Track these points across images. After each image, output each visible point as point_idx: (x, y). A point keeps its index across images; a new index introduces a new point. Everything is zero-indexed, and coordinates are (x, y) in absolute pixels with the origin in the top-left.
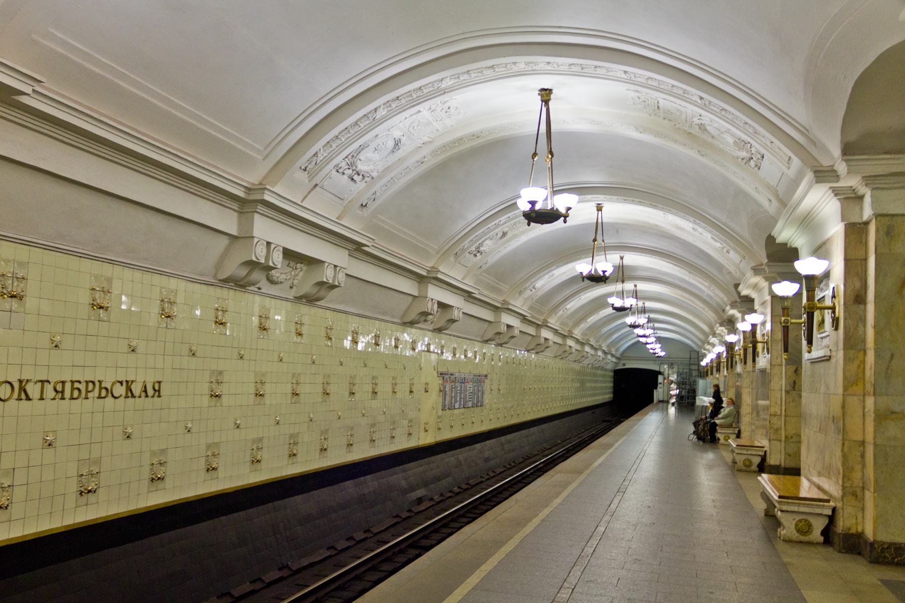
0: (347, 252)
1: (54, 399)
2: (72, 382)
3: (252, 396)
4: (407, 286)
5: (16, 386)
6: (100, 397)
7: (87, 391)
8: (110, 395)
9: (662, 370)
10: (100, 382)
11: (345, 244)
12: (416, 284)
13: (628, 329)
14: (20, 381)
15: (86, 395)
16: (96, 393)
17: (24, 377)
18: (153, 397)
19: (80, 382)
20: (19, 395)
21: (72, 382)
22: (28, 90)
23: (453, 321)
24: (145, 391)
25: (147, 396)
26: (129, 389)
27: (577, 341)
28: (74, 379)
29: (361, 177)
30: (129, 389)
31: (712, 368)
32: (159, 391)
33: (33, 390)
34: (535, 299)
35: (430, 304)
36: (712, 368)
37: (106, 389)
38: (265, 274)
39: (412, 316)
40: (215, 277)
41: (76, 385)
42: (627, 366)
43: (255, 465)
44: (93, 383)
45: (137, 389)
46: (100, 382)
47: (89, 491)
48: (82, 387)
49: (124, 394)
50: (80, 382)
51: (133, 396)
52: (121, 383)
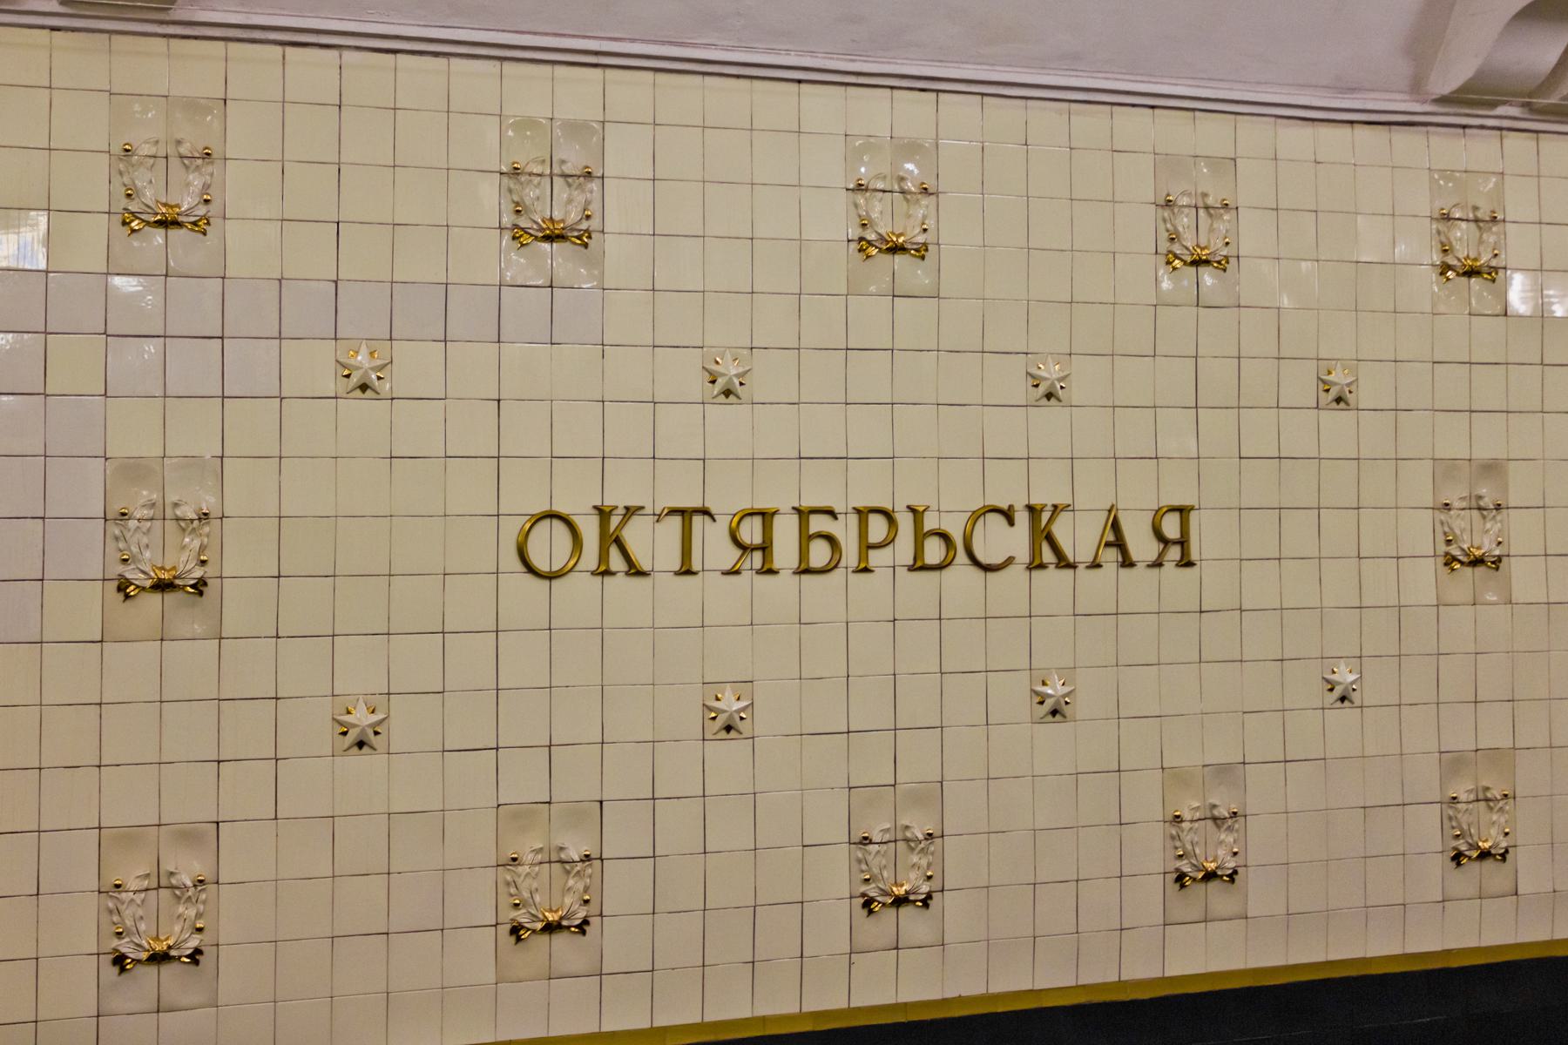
2: (803, 514)
6: (918, 566)
7: (866, 547)
8: (961, 557)
16: (904, 549)
17: (617, 498)
18: (1157, 564)
21: (803, 514)
24: (1119, 544)
26: (1043, 536)
33: (653, 542)
40: (1416, 87)
41: (818, 524)
44: (887, 515)
49: (1023, 555)
52: (1008, 515)
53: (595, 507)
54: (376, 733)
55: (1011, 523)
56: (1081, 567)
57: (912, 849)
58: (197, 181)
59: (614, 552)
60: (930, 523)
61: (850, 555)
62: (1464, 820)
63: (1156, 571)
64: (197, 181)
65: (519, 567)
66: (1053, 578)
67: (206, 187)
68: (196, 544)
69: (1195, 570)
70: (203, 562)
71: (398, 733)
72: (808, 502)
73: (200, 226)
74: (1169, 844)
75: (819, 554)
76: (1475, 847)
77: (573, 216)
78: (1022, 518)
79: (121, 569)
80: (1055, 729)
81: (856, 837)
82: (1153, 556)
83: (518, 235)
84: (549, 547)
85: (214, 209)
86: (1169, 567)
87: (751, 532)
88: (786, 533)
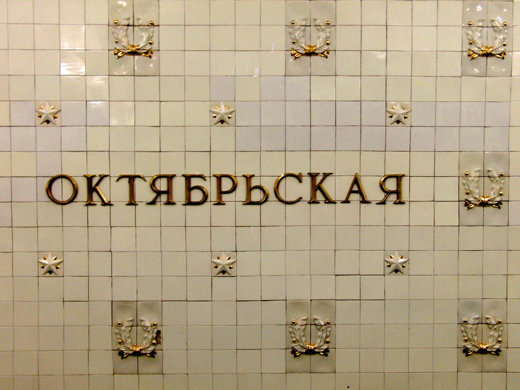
2: (188, 178)
6: (249, 202)
7: (221, 193)
10: (248, 178)
15: (220, 198)
16: (241, 193)
17: (96, 171)
20: (90, 197)
21: (188, 178)
26: (316, 188)
33: (114, 191)
38: (97, 188)
41: (195, 182)
46: (248, 178)
48: (210, 187)
49: (307, 197)
52: (299, 178)
53: (308, 174)
54: (403, 267)
55: (300, 181)
56: (338, 203)
57: (491, 329)
58: (323, 35)
59: (318, 193)
60: (255, 182)
61: (213, 196)
63: (383, 206)
64: (323, 35)
66: (322, 207)
67: (327, 38)
68: (498, 187)
69: (405, 207)
70: (501, 195)
71: (413, 268)
72: (189, 173)
73: (325, 54)
74: (289, 335)
75: (196, 196)
77: (497, 44)
78: (307, 181)
79: (466, 197)
81: (115, 323)
85: (331, 47)
86: (390, 204)
87: (162, 185)
88: (179, 185)
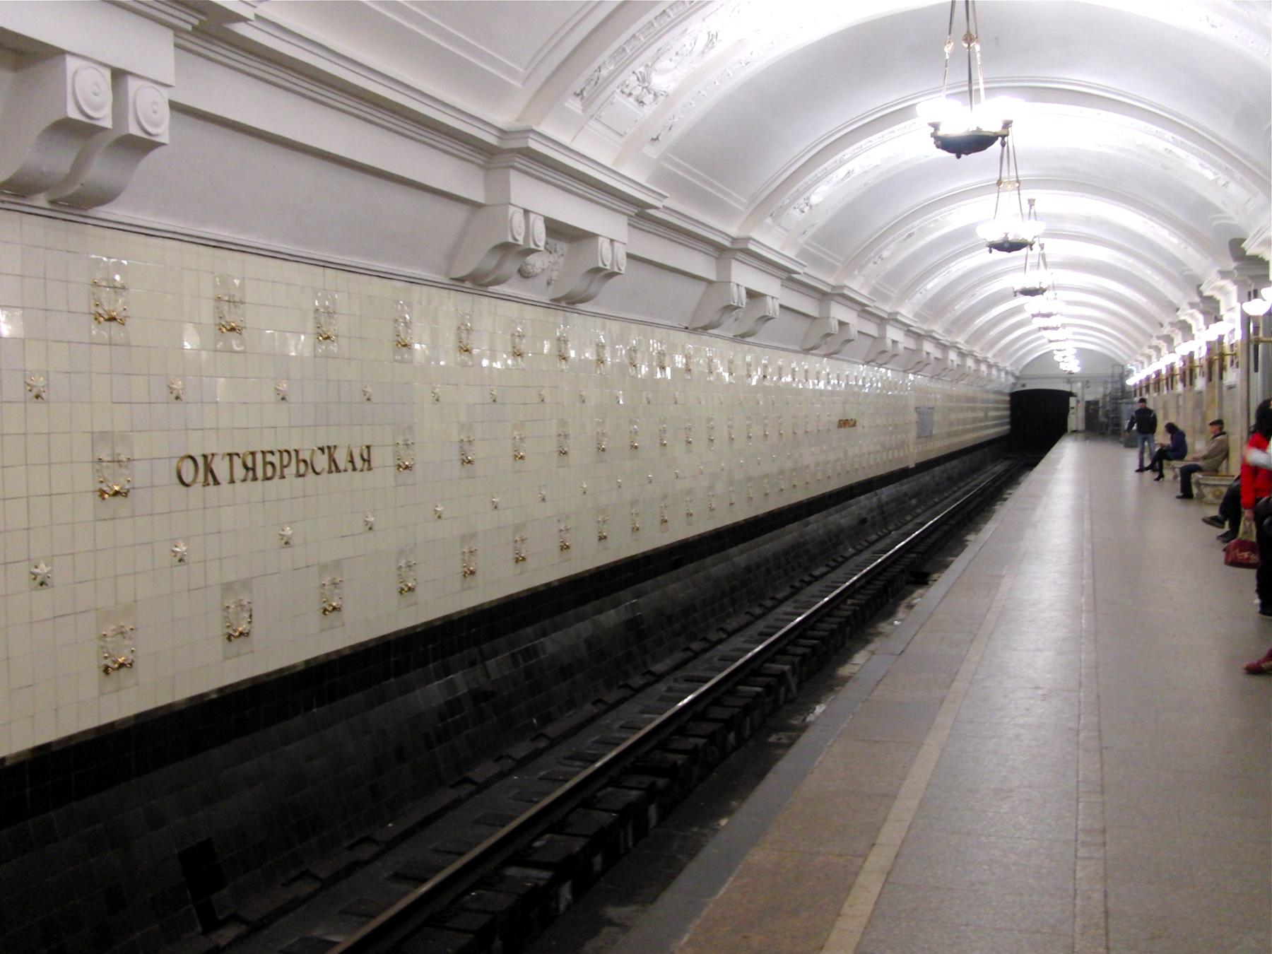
0: (168, 37)
1: (244, 480)
3: (392, 470)
4: (700, 264)
5: (200, 461)
6: (299, 475)
7: (283, 467)
8: (310, 470)
9: (1074, 391)
11: (779, 273)
12: (713, 262)
13: (985, 257)
14: (205, 457)
15: (282, 472)
17: (208, 452)
18: (244, 480)
19: (272, 453)
22: (659, 204)
23: (766, 319)
24: (352, 461)
25: (354, 469)
26: (332, 460)
27: (909, 331)
28: (265, 449)
29: (651, 96)
30: (332, 460)
31: (1141, 389)
32: (369, 461)
33: (220, 467)
34: (810, 232)
35: (518, 218)
36: (1141, 389)
37: (305, 461)
39: (708, 317)
40: (447, 274)
41: (269, 458)
42: (1028, 387)
43: (469, 578)
44: (288, 452)
45: (342, 460)
47: (122, 665)
49: (327, 468)
50: (272, 453)
51: (338, 470)
62: (110, 646)
65: (177, 481)
76: (115, 662)
80: (44, 592)
82: (242, 477)
83: (97, 317)
84: (188, 471)
